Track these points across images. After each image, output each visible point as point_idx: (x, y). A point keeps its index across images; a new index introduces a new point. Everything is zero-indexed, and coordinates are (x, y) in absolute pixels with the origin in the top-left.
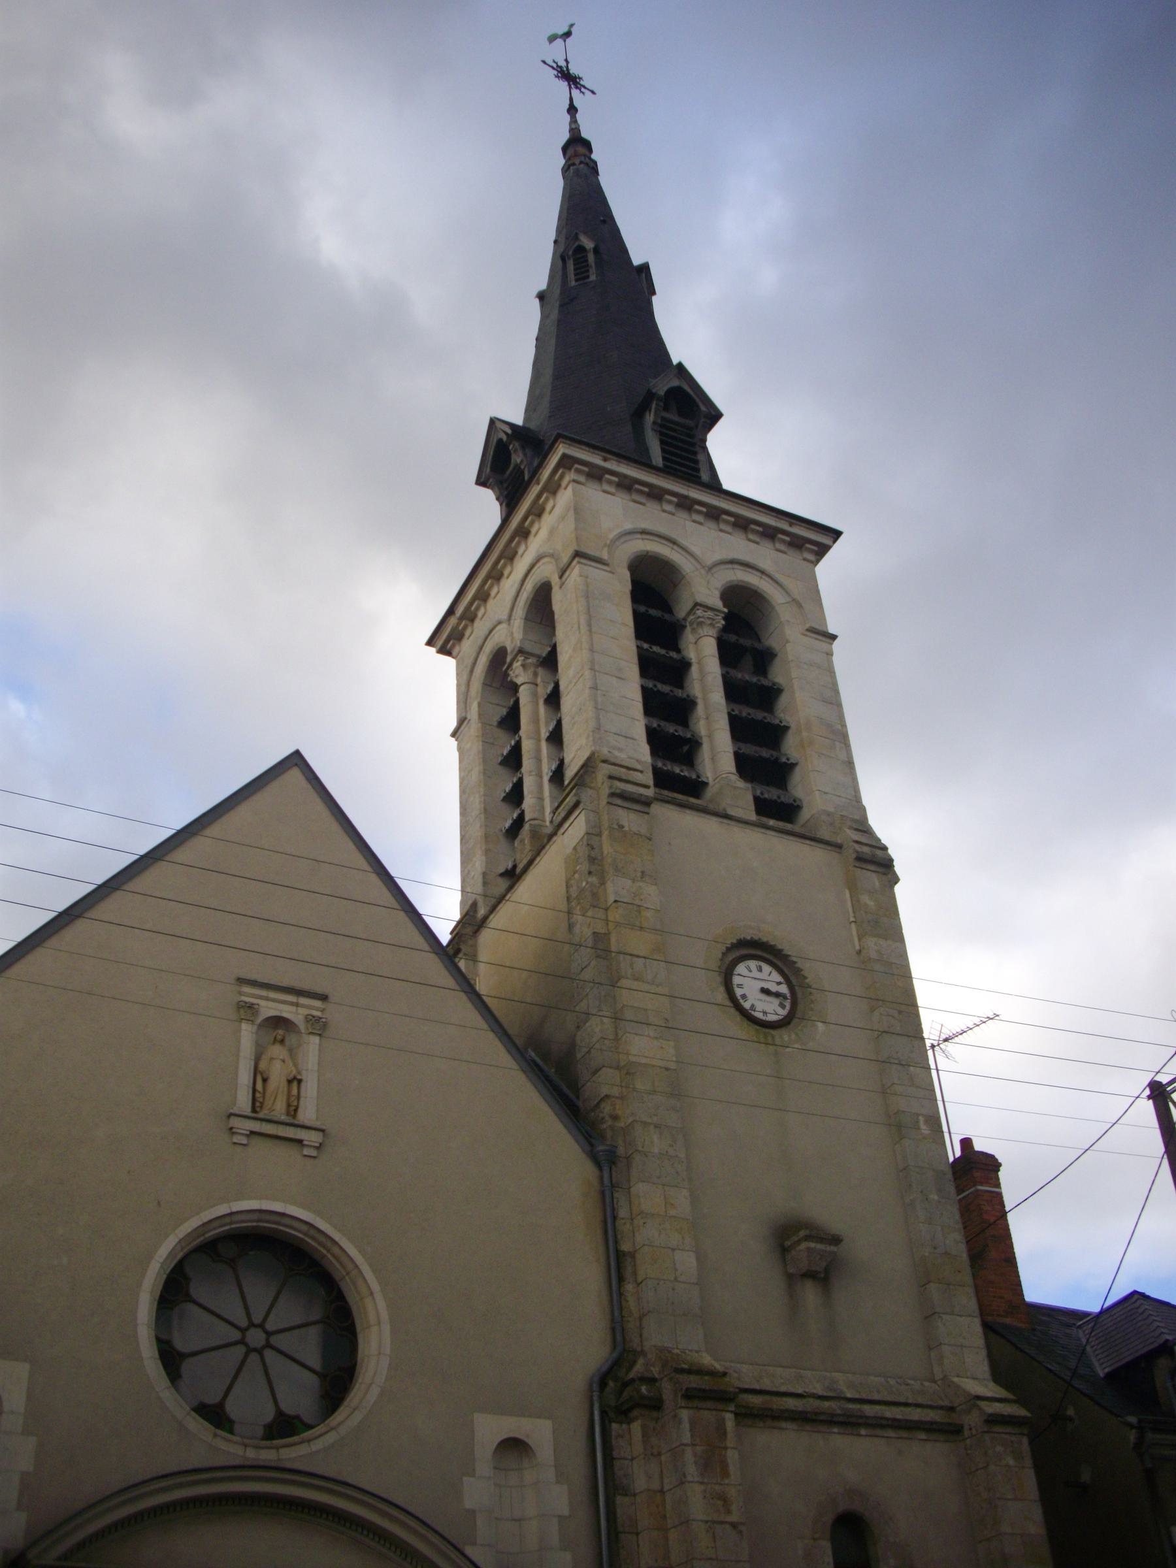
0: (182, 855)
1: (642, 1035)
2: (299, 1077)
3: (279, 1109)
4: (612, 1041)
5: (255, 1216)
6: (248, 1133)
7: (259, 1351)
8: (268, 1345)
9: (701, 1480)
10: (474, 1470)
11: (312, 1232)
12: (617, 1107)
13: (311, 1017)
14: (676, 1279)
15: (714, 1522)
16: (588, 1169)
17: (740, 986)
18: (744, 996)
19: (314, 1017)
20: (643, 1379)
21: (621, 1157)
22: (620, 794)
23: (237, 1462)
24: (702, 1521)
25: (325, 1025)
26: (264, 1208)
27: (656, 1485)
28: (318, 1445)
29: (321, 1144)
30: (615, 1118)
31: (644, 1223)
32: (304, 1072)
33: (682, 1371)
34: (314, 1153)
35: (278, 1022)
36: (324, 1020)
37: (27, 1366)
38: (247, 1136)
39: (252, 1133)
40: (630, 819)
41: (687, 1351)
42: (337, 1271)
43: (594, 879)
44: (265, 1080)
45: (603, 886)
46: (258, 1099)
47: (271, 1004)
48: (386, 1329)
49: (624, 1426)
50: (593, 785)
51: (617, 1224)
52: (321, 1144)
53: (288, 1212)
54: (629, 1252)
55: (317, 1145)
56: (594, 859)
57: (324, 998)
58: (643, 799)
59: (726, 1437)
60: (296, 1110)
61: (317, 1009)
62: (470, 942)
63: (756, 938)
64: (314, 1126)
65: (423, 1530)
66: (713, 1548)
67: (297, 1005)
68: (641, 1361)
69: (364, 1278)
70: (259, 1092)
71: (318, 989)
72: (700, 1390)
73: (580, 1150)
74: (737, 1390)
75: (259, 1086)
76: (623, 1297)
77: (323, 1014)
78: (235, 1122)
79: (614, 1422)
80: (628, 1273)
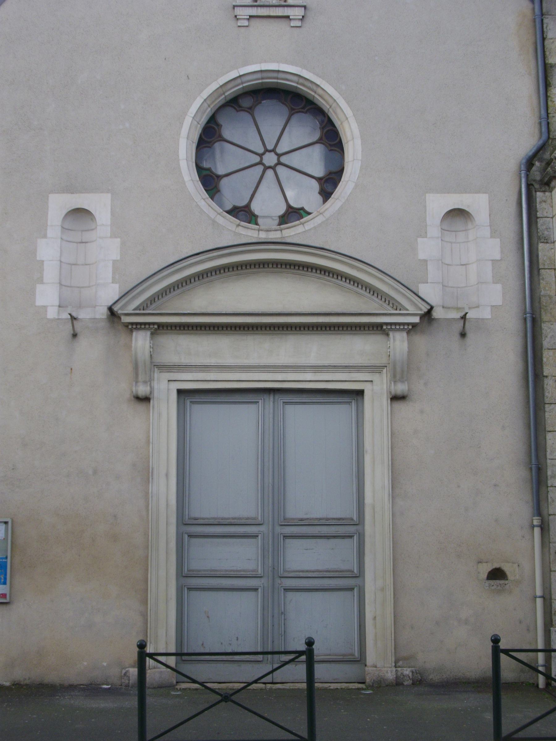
5: (259, 76)
6: (248, 17)
7: (273, 168)
8: (279, 163)
10: (426, 233)
11: (301, 81)
26: (263, 69)
28: (308, 226)
29: (303, 17)
34: (298, 23)
37: (109, 195)
38: (248, 19)
42: (325, 106)
48: (358, 142)
49: (547, 194)
53: (281, 69)
55: (301, 17)
64: (299, 4)
76: (549, 99)
78: (238, 11)
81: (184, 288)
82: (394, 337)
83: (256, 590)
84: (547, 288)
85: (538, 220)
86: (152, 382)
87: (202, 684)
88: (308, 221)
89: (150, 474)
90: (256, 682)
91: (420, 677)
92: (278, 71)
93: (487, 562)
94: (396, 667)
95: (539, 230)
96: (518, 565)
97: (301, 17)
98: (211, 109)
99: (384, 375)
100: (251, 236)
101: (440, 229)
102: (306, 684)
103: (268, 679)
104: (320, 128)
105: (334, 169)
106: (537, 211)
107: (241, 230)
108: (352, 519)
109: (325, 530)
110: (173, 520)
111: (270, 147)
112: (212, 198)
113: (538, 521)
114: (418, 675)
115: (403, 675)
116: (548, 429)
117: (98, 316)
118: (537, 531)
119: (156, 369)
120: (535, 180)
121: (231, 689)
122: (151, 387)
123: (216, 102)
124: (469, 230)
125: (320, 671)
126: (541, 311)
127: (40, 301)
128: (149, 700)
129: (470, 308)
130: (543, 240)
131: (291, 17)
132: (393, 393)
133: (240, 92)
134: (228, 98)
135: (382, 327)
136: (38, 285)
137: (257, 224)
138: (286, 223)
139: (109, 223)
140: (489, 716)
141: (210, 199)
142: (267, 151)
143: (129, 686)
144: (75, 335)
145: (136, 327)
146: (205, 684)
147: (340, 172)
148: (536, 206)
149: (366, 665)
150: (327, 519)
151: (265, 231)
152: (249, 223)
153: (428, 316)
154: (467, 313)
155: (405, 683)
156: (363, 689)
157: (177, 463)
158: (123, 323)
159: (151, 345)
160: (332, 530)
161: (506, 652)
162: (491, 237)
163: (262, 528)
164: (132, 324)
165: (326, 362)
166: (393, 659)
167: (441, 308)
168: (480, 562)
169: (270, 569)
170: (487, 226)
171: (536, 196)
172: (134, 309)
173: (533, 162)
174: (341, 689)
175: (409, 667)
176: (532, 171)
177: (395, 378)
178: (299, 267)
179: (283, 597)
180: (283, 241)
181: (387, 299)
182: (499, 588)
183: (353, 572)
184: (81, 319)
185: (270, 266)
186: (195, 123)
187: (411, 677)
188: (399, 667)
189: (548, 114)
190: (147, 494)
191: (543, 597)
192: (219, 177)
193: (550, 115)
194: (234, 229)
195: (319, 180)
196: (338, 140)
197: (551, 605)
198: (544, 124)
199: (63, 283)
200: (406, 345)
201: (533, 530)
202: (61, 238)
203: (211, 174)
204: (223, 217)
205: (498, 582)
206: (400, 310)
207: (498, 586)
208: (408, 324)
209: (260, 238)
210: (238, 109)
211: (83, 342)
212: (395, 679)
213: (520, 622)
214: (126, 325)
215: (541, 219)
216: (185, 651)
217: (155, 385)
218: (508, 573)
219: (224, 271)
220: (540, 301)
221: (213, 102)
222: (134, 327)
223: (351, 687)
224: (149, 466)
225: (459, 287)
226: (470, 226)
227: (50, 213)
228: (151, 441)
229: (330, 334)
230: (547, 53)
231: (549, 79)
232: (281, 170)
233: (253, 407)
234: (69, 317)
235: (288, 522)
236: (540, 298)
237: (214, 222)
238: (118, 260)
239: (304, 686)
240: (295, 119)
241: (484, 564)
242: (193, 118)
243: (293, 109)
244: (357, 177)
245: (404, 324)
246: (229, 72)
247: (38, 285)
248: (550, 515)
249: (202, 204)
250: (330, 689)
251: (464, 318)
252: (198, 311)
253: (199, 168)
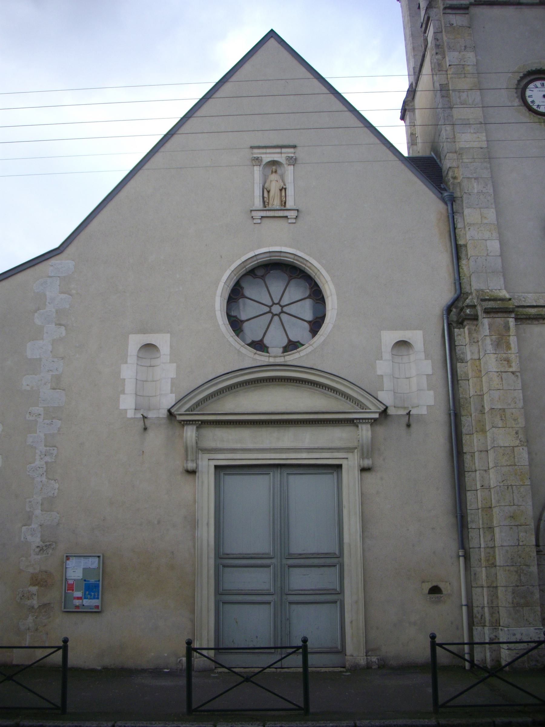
0: (220, 93)
1: (466, 133)
2: (284, 187)
3: (276, 203)
4: (452, 139)
5: (268, 255)
6: (260, 217)
8: (282, 312)
9: (495, 352)
11: (296, 258)
12: (456, 172)
13: (288, 158)
14: (487, 255)
15: (501, 372)
16: (441, 206)
17: (530, 96)
18: (533, 102)
19: (289, 157)
20: (468, 306)
21: (458, 197)
22: (449, 7)
23: (266, 364)
24: (495, 372)
25: (296, 159)
27: (476, 357)
28: (302, 354)
29: (297, 216)
30: (455, 178)
31: (469, 229)
32: (287, 184)
33: (485, 300)
34: (294, 221)
35: (274, 163)
37: (169, 335)
38: (261, 219)
39: (262, 217)
40: (457, 20)
41: (494, 290)
42: (312, 274)
43: (439, 57)
44: (269, 192)
45: (444, 59)
46: (266, 201)
47: (268, 155)
48: (335, 297)
49: (462, 330)
50: (436, 6)
51: (456, 231)
54: (463, 245)
56: (439, 45)
57: (294, 147)
58: (463, 6)
59: (510, 330)
60: (285, 203)
61: (291, 153)
62: (411, 104)
63: (539, 68)
64: (293, 209)
65: (352, 386)
66: (500, 384)
67: (281, 153)
68: (470, 297)
69: (322, 275)
70: (266, 198)
71: (291, 144)
72: (492, 308)
73: (436, 197)
74: (514, 307)
75: (266, 195)
76: (460, 267)
78: (254, 214)
79: (456, 328)
80: (463, 256)
81: (219, 396)
82: (361, 427)
83: (269, 603)
84: (464, 393)
85: (456, 347)
86: (198, 460)
87: (229, 669)
88: (302, 350)
89: (196, 524)
90: (269, 667)
91: (383, 663)
92: (281, 252)
93: (428, 582)
94: (366, 656)
95: (457, 354)
96: (450, 584)
97: (295, 217)
98: (237, 277)
99: (356, 454)
100: (264, 361)
101: (391, 354)
102: (302, 668)
103: (278, 665)
104: (309, 288)
105: (320, 315)
106: (455, 342)
107: (257, 357)
108: (335, 554)
109: (316, 562)
110: (212, 555)
111: (276, 301)
112: (238, 335)
113: (463, 552)
114: (382, 661)
115: (372, 662)
116: (467, 489)
117: (161, 416)
118: (462, 559)
119: (200, 452)
120: (453, 321)
121: (252, 672)
122: (196, 464)
123: (240, 272)
124: (411, 354)
125: (312, 660)
126: (460, 408)
127: (122, 407)
128: (194, 680)
129: (412, 407)
130: (460, 361)
131: (289, 217)
132: (362, 465)
133: (257, 265)
134: (248, 270)
135: (353, 421)
136: (121, 395)
137: (268, 352)
138: (287, 352)
139: (169, 354)
140: (430, 690)
141: (236, 336)
142: (274, 304)
143: (182, 670)
144: (145, 429)
145: (187, 423)
146: (232, 669)
147: (323, 318)
148: (454, 338)
149: (346, 655)
150: (318, 554)
151: (273, 357)
152: (263, 352)
153: (384, 413)
154: (410, 411)
155: (373, 667)
156: (343, 672)
157: (215, 514)
158: (178, 420)
159: (197, 435)
160: (321, 561)
161: (440, 645)
162: (426, 359)
163: (273, 561)
164: (184, 421)
165: (316, 446)
166: (365, 650)
167: (393, 408)
168: (423, 582)
169: (279, 589)
170: (422, 352)
171: (454, 332)
172: (185, 411)
173: (451, 309)
174: (329, 672)
175: (376, 656)
176: (450, 315)
177: (363, 456)
178: (296, 381)
179: (288, 607)
180: (286, 364)
181: (357, 402)
182: (437, 599)
183: (336, 590)
184: (150, 418)
185: (277, 380)
186: (226, 286)
187: (377, 663)
188: (369, 656)
189: (460, 277)
190: (194, 537)
191: (467, 605)
192: (243, 322)
193: (461, 278)
194: (252, 357)
195: (309, 322)
196: (322, 295)
197: (473, 611)
198: (457, 283)
199: (138, 394)
200: (369, 433)
201: (459, 559)
202: (137, 364)
203: (237, 319)
204: (245, 348)
205: (436, 595)
206: (365, 409)
207: (436, 598)
208: (371, 419)
209: (270, 362)
210: (254, 276)
211: (151, 434)
212: (366, 664)
213: (452, 623)
214: (180, 422)
215: (458, 346)
216: (221, 647)
217: (200, 463)
218: (443, 589)
219: (246, 384)
220: (459, 402)
221: (238, 272)
222: (185, 423)
223: (335, 670)
224: (195, 519)
225: (405, 393)
226: (411, 352)
227: (129, 347)
228: (197, 501)
229: (318, 426)
230: (458, 238)
231: (459, 254)
232: (284, 317)
233: (266, 477)
234: (142, 416)
235: (291, 556)
236: (459, 400)
237: (239, 351)
238: (174, 378)
239: (301, 670)
240: (293, 282)
241: (426, 583)
242: (225, 283)
243: (291, 276)
244: (334, 321)
245: (368, 419)
246: (248, 252)
247: (121, 395)
248: (470, 548)
249: (231, 340)
250: (321, 672)
251: (409, 414)
252: (229, 412)
253: (229, 316)
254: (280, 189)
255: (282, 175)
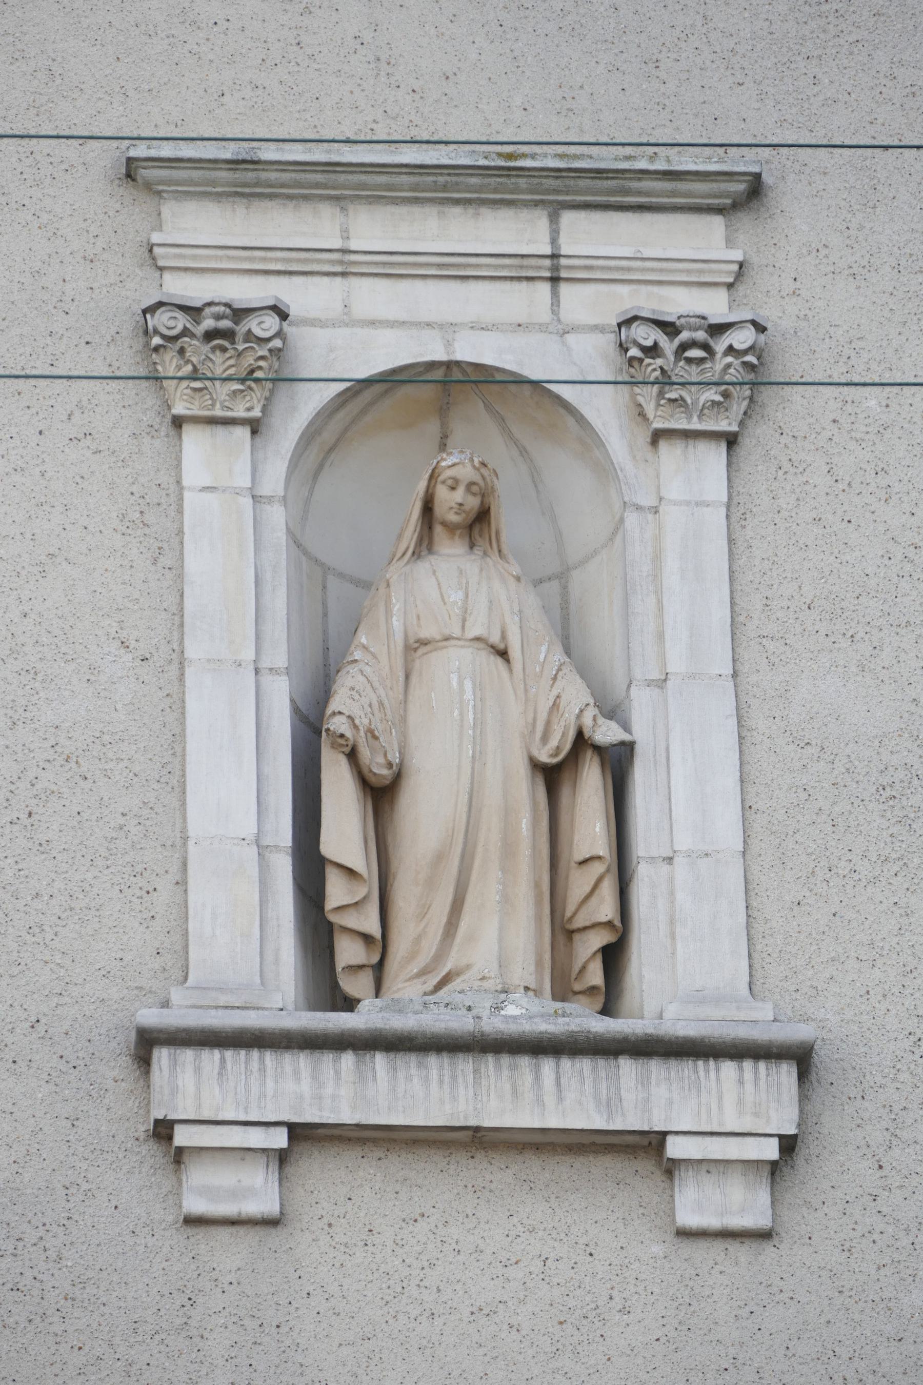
6: (279, 1139)
13: (647, 335)
19: (669, 328)
29: (788, 1144)
36: (742, 338)
46: (350, 920)
52: (788, 1144)
64: (743, 1033)
77: (732, 304)
97: (770, 1151)
131: (676, 1148)
254: (536, 766)
255: (562, 576)
